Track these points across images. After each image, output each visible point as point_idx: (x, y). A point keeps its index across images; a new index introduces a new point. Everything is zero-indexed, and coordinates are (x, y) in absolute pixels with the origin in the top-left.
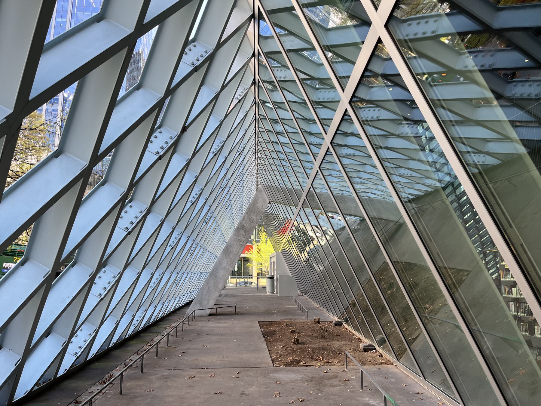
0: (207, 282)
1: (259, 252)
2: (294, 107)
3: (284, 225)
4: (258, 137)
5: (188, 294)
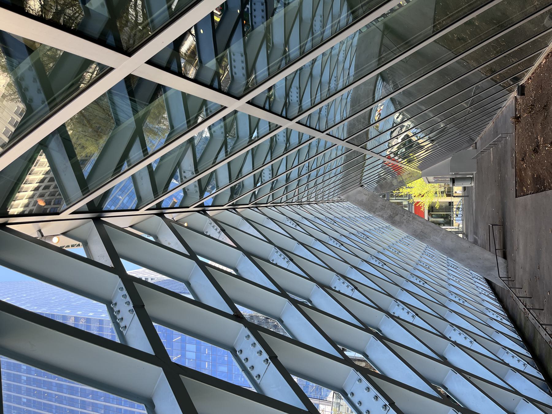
0: (460, 260)
1: (422, 195)
2: (259, 162)
3: (390, 168)
4: (281, 203)
5: (475, 282)
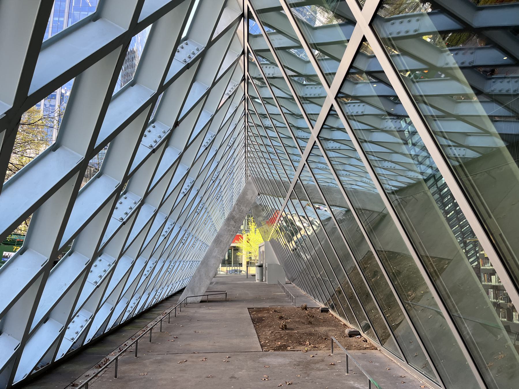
0: (199, 270)
1: (249, 241)
2: (282, 102)
3: (272, 216)
4: (248, 131)
5: (180, 281)
